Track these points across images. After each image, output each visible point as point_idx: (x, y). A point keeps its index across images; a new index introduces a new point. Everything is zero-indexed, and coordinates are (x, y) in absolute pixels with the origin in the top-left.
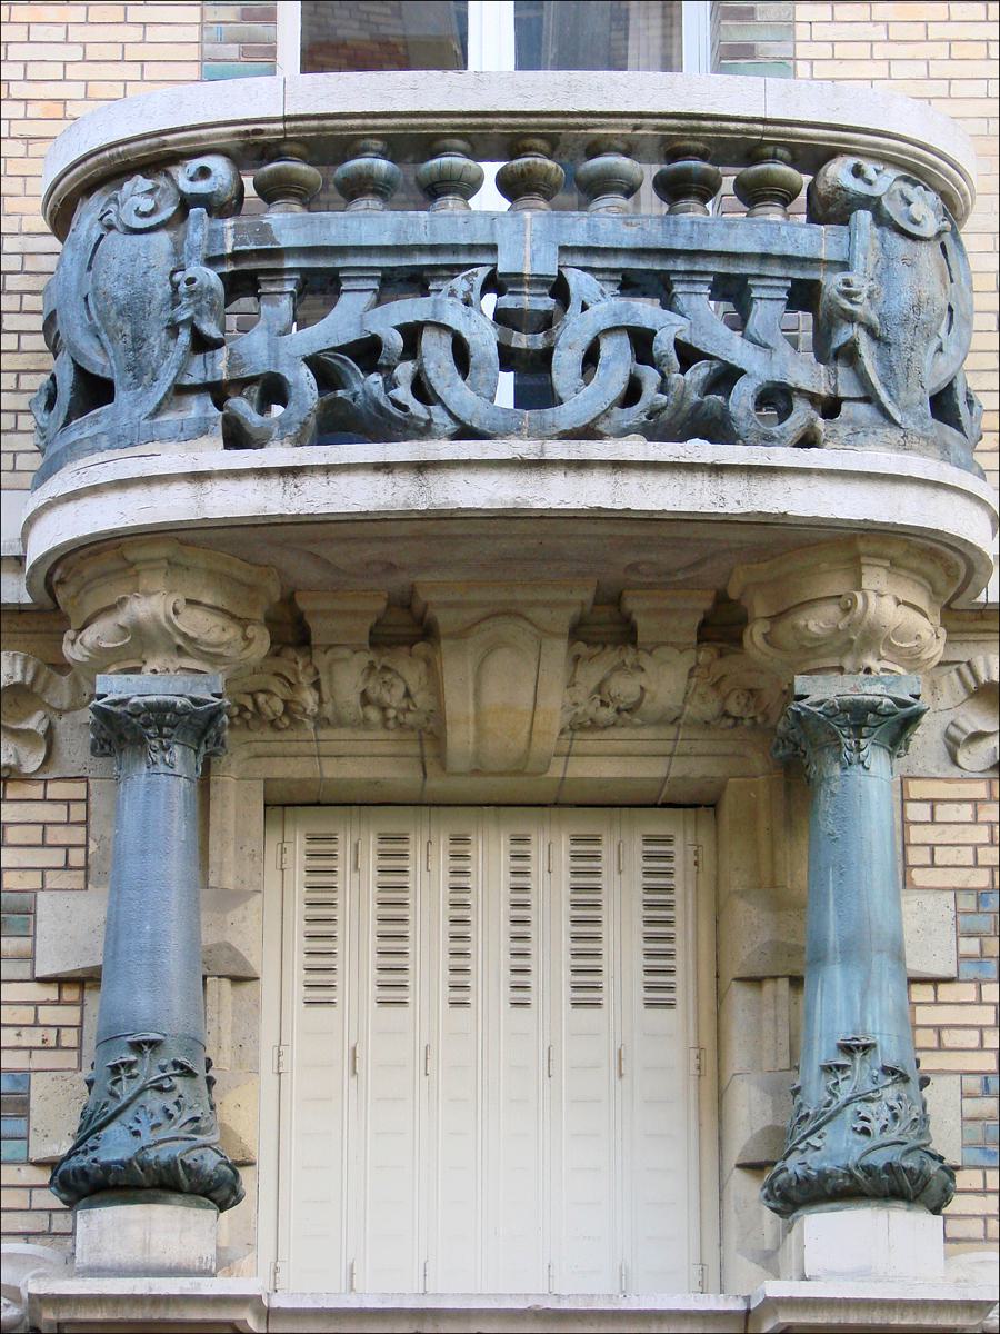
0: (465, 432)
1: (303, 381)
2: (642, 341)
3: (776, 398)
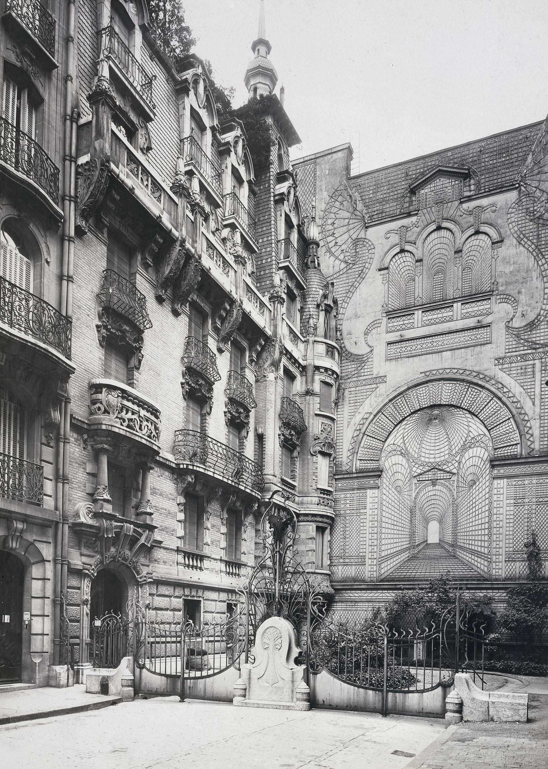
0: (137, 431)
1: (127, 420)
2: (148, 426)
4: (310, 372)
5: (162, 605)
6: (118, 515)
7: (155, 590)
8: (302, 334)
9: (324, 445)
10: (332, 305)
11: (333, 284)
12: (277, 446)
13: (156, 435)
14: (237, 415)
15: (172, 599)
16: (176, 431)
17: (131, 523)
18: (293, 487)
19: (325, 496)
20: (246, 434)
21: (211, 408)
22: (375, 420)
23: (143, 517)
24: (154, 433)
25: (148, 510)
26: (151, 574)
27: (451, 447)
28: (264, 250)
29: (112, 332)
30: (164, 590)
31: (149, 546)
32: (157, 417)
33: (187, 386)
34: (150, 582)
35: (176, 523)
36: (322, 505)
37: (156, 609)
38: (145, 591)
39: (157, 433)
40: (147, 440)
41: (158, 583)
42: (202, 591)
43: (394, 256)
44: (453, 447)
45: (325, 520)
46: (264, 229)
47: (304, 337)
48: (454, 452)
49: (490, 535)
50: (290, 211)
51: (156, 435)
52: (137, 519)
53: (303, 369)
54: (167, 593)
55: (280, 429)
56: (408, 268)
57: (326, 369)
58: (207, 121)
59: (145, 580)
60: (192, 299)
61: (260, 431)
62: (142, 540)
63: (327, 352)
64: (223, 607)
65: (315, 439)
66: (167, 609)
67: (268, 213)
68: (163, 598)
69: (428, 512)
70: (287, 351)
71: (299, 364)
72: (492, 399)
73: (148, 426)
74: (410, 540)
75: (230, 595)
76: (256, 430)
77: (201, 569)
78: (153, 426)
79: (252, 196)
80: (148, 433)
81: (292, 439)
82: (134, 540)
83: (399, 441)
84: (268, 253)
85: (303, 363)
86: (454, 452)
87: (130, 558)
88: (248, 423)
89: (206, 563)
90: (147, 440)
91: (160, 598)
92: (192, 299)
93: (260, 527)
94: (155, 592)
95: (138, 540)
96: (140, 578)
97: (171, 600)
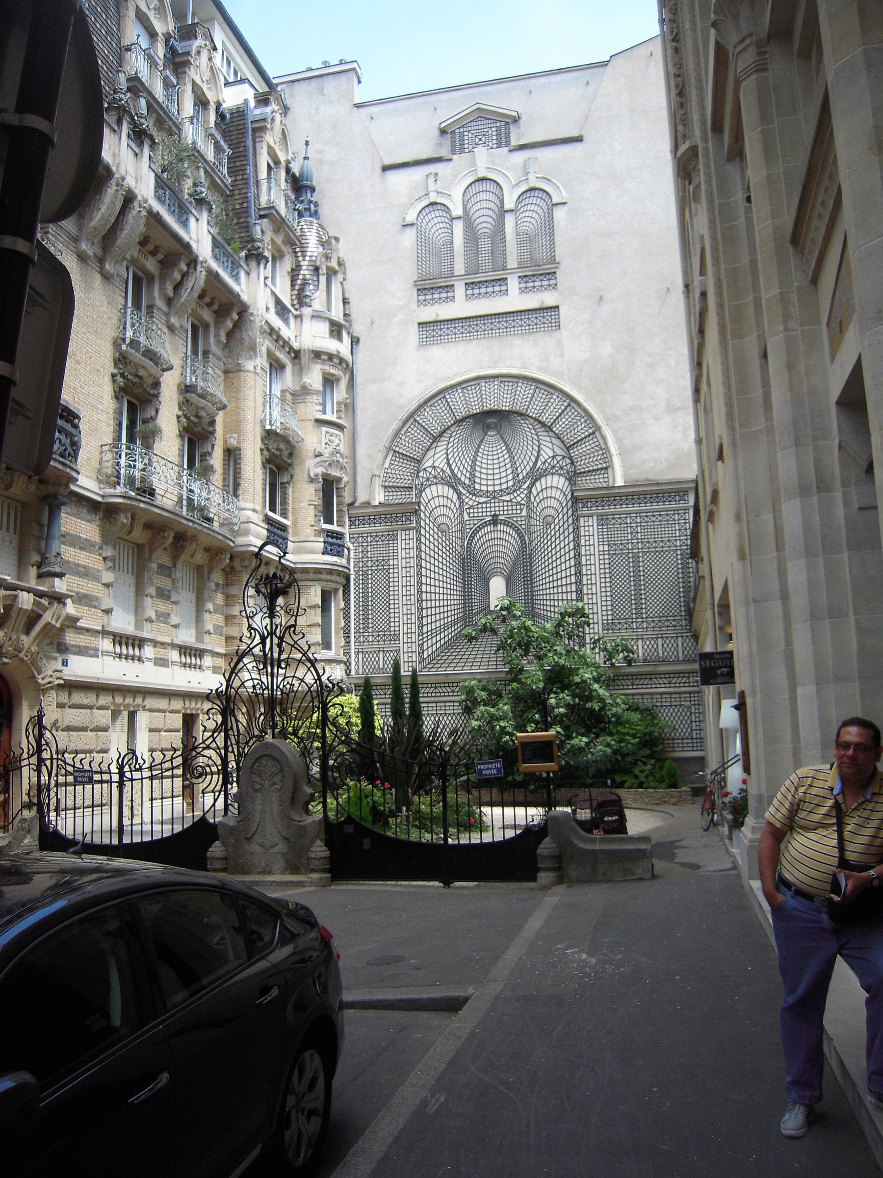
3: (69, 455)
4: (305, 359)
5: (76, 723)
6: (8, 578)
7: (67, 697)
8: (293, 305)
9: (330, 465)
10: (337, 268)
11: (337, 239)
12: (259, 465)
13: (72, 454)
14: (195, 420)
15: (95, 711)
16: (102, 446)
17: (29, 590)
18: (284, 528)
19: (334, 541)
20: (153, 413)
21: (157, 411)
22: (405, 429)
23: (48, 580)
24: (70, 450)
25: (57, 569)
26: (61, 671)
27: (518, 475)
28: (237, 192)
29: (128, 380)
30: (79, 698)
31: (58, 625)
32: (76, 427)
33: (121, 379)
34: (59, 685)
35: (100, 587)
36: (329, 554)
37: (68, 729)
38: (50, 699)
39: (74, 450)
40: (60, 462)
41: (71, 686)
42: (142, 696)
43: (424, 208)
44: (519, 470)
45: (334, 578)
46: (238, 164)
47: (296, 310)
48: (521, 477)
49: (578, 574)
50: (275, 143)
51: (72, 454)
52: (37, 584)
53: (296, 355)
54: (85, 701)
55: (262, 441)
56: (443, 230)
57: (331, 357)
58: (159, 27)
59: (50, 683)
60: (132, 256)
61: (233, 442)
62: (47, 617)
63: (331, 332)
64: (177, 721)
65: (316, 456)
66: (84, 729)
67: (242, 145)
68: (79, 711)
69: (488, 564)
70: (272, 329)
71: (291, 348)
72: (569, 405)
73: (60, 440)
74: (465, 603)
75: (187, 703)
76: (225, 441)
77: (140, 659)
78: (69, 440)
79: (202, 99)
80: (61, 450)
81: (281, 455)
82: (33, 618)
83: (441, 463)
84: (242, 196)
85: (296, 346)
86: (521, 477)
87: (26, 646)
88: (212, 433)
89: (148, 651)
90: (60, 462)
91: (74, 711)
92: (132, 256)
93: (235, 590)
94: (66, 701)
95: (40, 616)
96: (43, 679)
97: (92, 713)
